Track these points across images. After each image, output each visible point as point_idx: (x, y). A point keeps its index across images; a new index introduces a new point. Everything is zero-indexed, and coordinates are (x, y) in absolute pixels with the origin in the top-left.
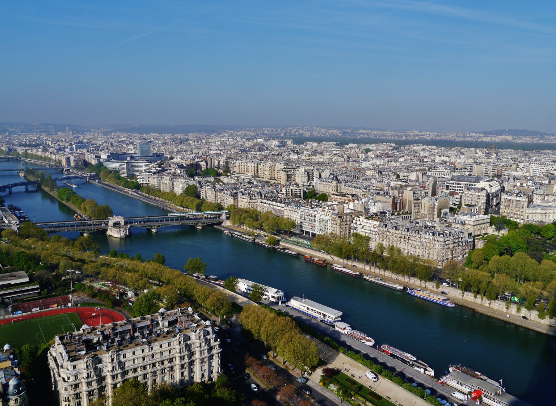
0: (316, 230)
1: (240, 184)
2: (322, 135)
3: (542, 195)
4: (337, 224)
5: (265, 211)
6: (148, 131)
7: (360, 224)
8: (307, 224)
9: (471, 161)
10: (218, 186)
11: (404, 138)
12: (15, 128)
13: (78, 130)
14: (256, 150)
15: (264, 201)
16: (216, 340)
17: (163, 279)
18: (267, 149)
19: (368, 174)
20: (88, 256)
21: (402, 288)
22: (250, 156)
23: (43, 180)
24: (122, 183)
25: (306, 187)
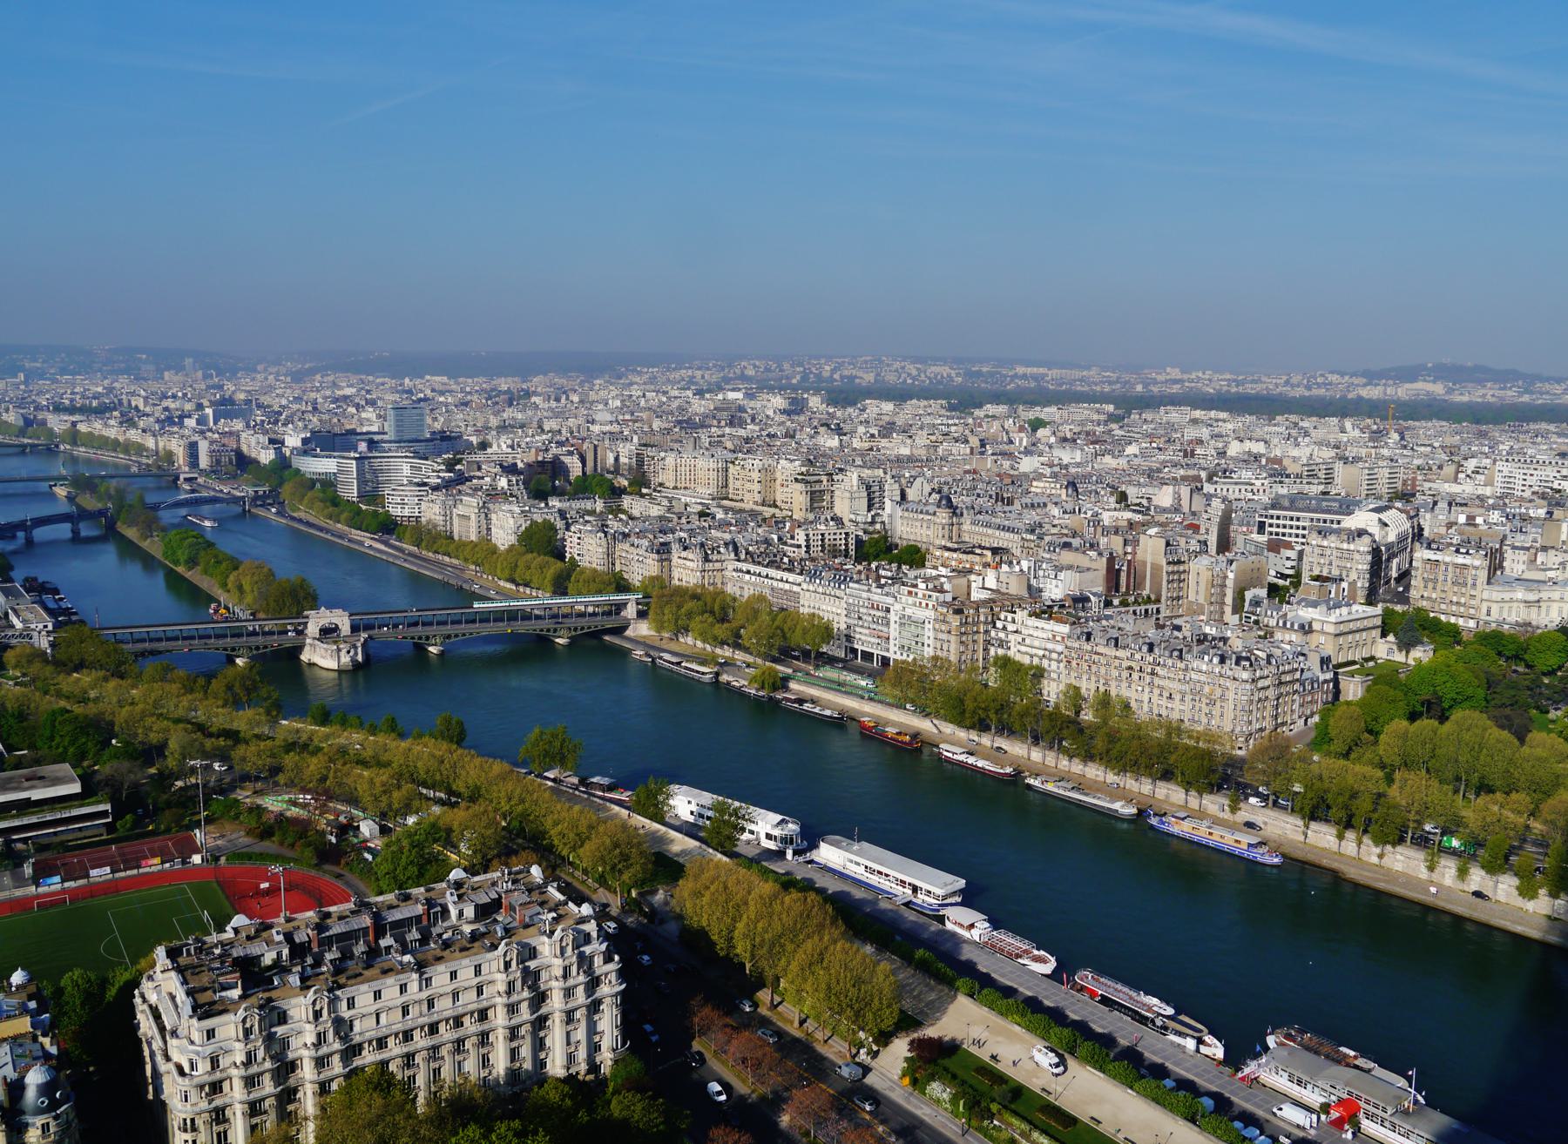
0: (892, 648)
1: (676, 519)
2: (909, 381)
3: (1528, 549)
4: (949, 632)
5: (746, 596)
6: (419, 368)
7: (1016, 632)
8: (867, 631)
9: (1328, 454)
10: (614, 525)
11: (1139, 388)
12: (43, 362)
13: (220, 365)
14: (723, 423)
15: (745, 566)
16: (608, 959)
17: (459, 786)
18: (753, 420)
19: (1038, 490)
20: (249, 722)
21: (1134, 811)
22: (705, 441)
23: (120, 508)
24: (343, 516)
25: (862, 526)
